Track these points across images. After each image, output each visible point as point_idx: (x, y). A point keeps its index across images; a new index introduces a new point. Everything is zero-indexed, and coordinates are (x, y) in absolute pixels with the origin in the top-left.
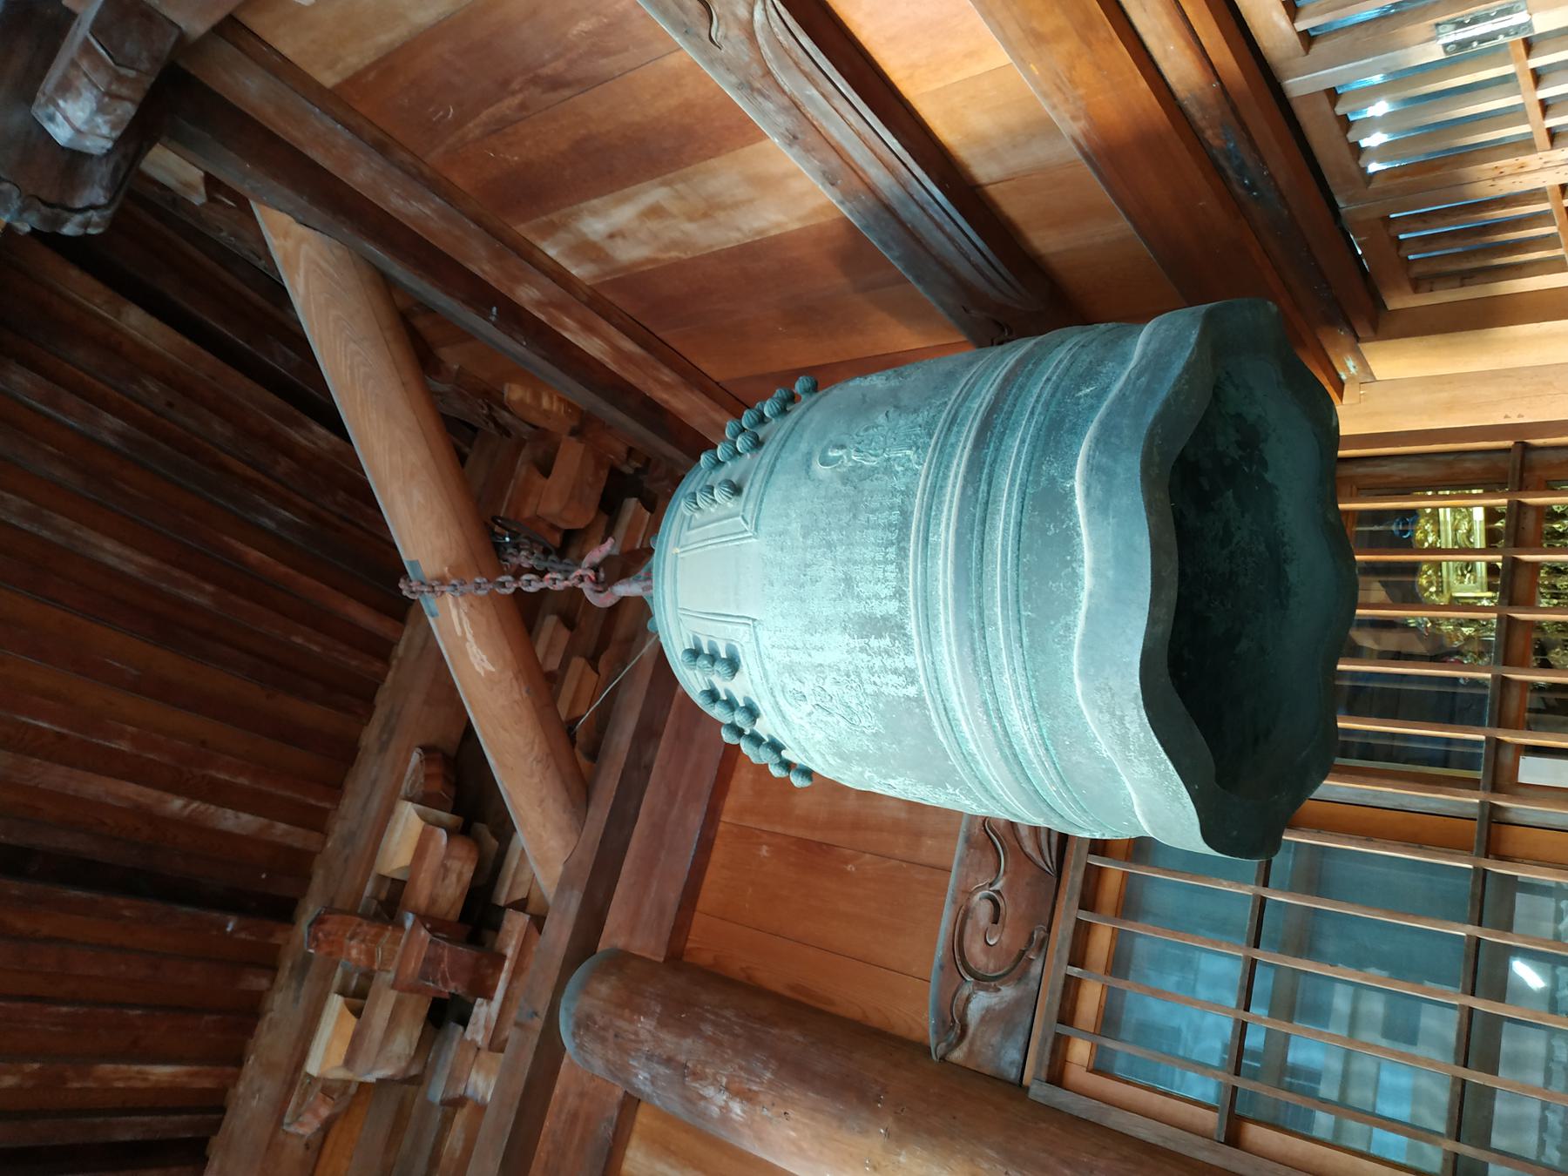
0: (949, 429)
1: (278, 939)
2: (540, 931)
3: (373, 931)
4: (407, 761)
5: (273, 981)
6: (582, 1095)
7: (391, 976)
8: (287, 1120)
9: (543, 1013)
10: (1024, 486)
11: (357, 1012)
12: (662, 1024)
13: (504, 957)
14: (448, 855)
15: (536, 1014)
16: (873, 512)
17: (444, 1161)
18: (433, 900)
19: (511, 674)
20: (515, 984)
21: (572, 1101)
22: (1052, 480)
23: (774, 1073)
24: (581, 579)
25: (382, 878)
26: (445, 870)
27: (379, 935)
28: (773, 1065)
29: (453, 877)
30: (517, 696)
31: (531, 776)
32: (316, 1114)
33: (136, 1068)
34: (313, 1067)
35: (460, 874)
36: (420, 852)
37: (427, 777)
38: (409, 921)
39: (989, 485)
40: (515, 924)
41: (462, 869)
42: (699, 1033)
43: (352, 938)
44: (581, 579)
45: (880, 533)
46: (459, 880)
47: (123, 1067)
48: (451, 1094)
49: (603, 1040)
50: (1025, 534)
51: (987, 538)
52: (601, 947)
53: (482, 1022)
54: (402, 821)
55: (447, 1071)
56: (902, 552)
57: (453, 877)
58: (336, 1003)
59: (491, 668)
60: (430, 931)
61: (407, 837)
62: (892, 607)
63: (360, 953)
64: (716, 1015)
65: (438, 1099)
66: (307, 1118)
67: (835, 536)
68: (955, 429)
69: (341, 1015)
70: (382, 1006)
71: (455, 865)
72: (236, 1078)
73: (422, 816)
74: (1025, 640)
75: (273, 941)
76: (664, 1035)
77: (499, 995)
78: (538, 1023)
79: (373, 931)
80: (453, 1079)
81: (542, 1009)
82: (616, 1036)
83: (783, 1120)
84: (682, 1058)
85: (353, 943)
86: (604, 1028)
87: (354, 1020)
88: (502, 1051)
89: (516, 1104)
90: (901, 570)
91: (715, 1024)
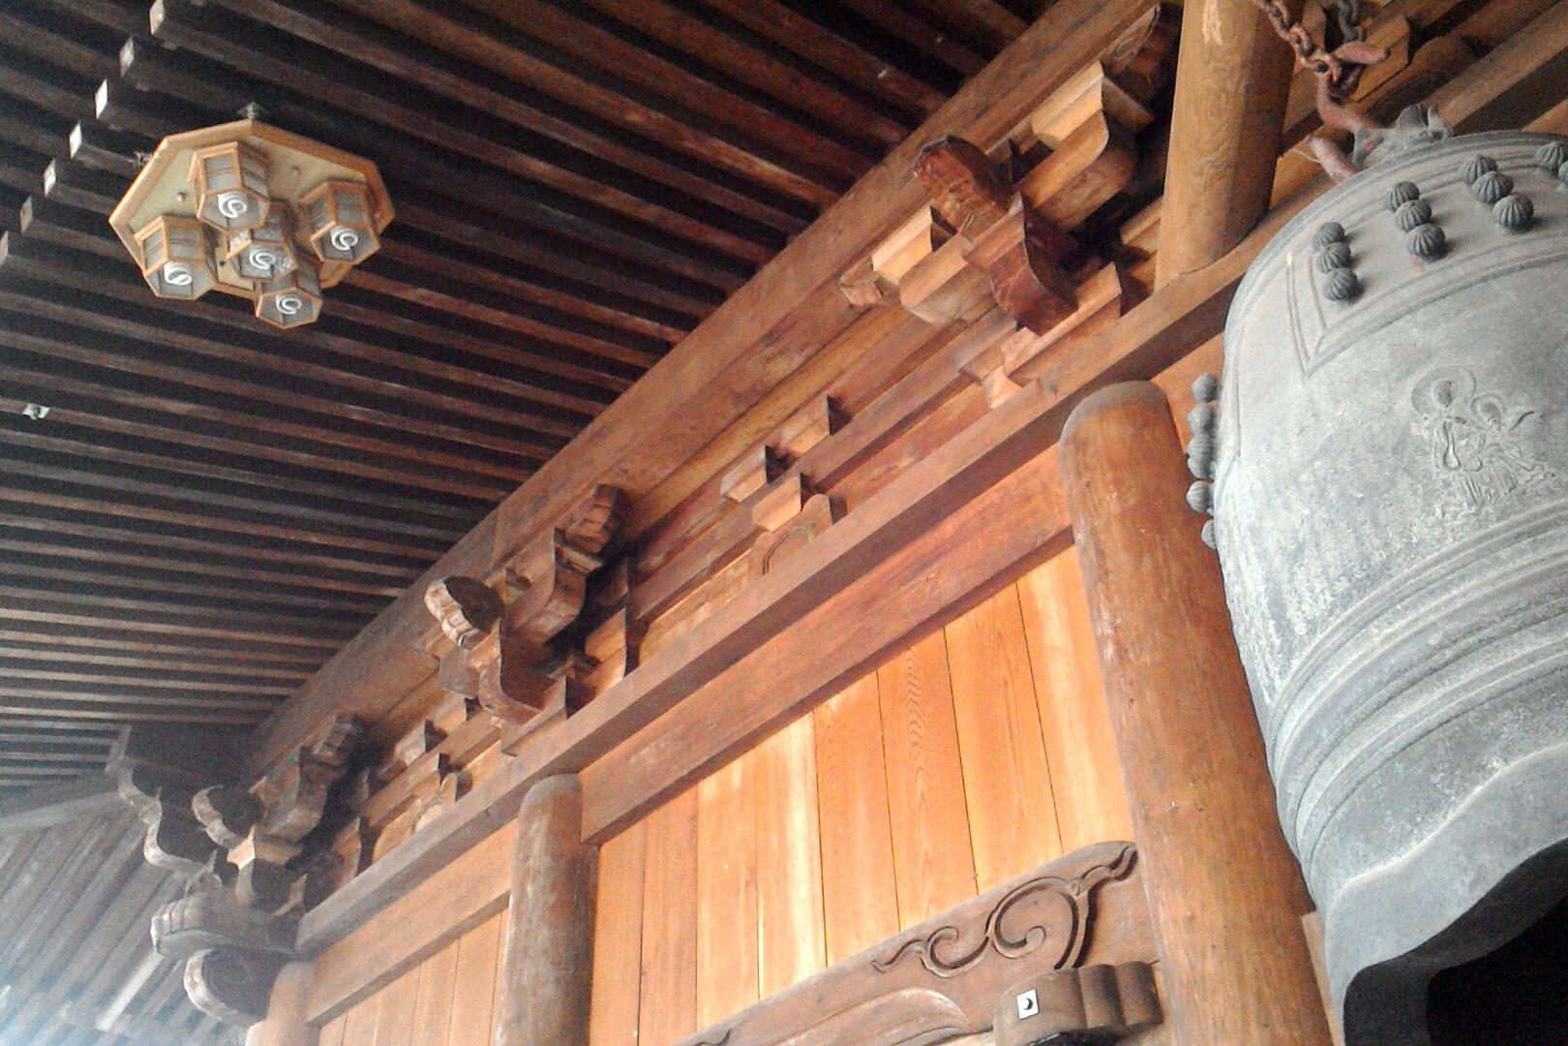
0: (1519, 536)
1: (928, 103)
2: (1123, 313)
3: (975, 197)
4: (1140, 13)
5: (904, 138)
6: (1045, 488)
7: (969, 246)
8: (843, 279)
9: (1061, 397)
10: (1471, 706)
11: (937, 242)
12: (1123, 516)
13: (1075, 307)
14: (1092, 168)
15: (1055, 390)
16: (1375, 524)
17: (940, 411)
18: (1052, 201)
19: (1237, 59)
20: (1067, 341)
21: (1034, 485)
22: (1495, 735)
23: (1153, 662)
24: (1324, 68)
25: (1029, 132)
26: (1082, 178)
27: (977, 204)
28: (1159, 655)
29: (1086, 191)
30: (1230, 86)
31: (1201, 174)
32: (864, 292)
33: (744, 154)
34: (880, 258)
35: (1096, 191)
36: (1077, 137)
37: (1143, 51)
38: (1017, 207)
39: (1457, 657)
40: (1107, 285)
41: (1104, 189)
42: (1137, 563)
43: (951, 191)
44: (1324, 68)
45: (1354, 554)
46: (1090, 196)
47: (735, 149)
48: (973, 370)
49: (1079, 475)
50: (1420, 747)
51: (1399, 700)
52: (1157, 380)
53: (1021, 346)
54: (1079, 92)
55: (981, 348)
56: (1346, 599)
57: (1086, 191)
58: (923, 220)
59: (1219, 40)
60: (1028, 232)
61: (1074, 111)
62: (1300, 628)
63: (953, 208)
64: (1166, 559)
65: (961, 365)
66: (855, 292)
67: (1333, 493)
68: (1525, 543)
69: (921, 236)
70: (952, 262)
71: (1095, 181)
72: (832, 202)
73: (1106, 96)
74: (1339, 815)
75: (921, 102)
76: (1116, 528)
77: (1049, 337)
78: (1051, 401)
79: (975, 197)
80: (981, 358)
81: (1068, 388)
82: (1088, 485)
83: (1127, 700)
84: (1110, 565)
85: (951, 196)
86: (1087, 467)
87: (929, 247)
88: (1022, 385)
89: (990, 448)
90: (1331, 612)
91: (1156, 566)
